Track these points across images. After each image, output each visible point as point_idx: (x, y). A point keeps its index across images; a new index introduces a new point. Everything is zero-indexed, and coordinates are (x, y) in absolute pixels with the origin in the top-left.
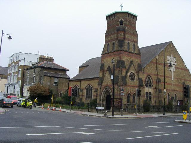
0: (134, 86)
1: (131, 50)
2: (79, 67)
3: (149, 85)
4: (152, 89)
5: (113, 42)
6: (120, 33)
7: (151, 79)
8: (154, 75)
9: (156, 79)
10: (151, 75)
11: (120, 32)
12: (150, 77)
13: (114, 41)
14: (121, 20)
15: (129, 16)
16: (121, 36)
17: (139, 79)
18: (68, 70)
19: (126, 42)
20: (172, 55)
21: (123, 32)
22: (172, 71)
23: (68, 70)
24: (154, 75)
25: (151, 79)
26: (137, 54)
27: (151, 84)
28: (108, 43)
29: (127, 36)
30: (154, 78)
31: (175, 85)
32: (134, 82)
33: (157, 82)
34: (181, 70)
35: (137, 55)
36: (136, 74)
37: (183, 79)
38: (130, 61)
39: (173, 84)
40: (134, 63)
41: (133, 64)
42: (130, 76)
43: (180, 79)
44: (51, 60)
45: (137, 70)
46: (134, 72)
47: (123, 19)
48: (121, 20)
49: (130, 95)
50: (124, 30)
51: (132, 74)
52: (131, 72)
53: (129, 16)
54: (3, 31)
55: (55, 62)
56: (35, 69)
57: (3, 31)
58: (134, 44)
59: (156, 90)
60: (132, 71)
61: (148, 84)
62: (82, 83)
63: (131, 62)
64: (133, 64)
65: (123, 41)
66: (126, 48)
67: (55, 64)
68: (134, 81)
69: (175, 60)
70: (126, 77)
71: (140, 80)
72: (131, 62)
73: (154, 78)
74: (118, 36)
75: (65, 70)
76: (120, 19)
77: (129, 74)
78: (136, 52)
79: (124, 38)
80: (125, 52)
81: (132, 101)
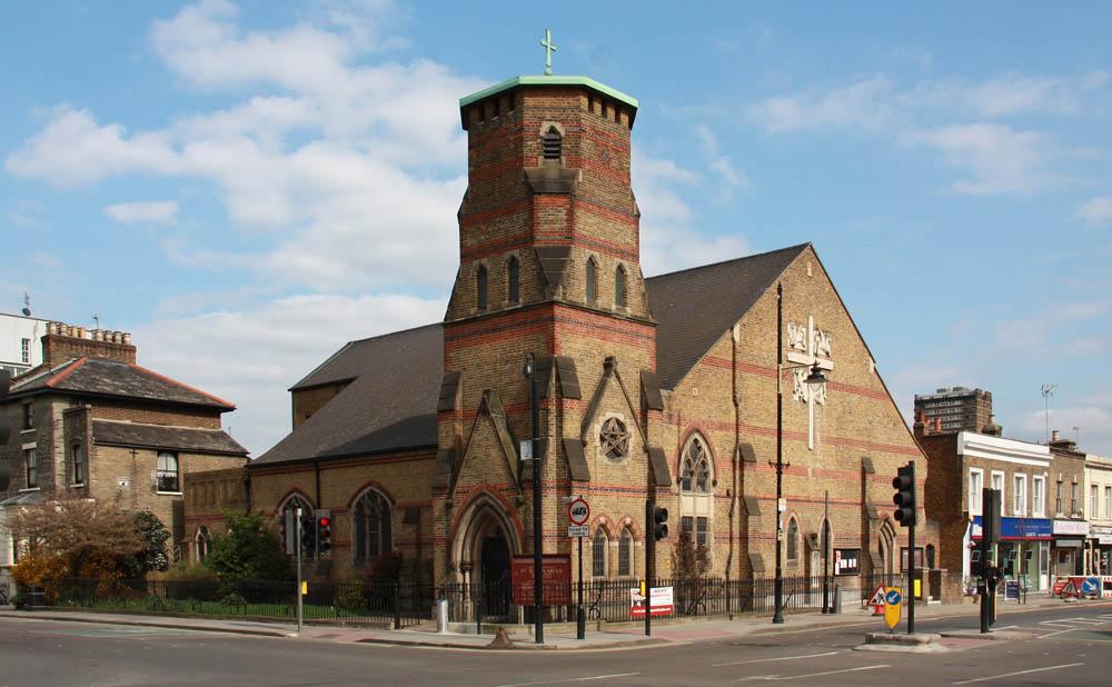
0: (623, 490)
1: (607, 300)
2: (295, 391)
4: (712, 498)
5: (507, 255)
6: (547, 204)
7: (704, 447)
8: (722, 427)
9: (731, 447)
10: (703, 429)
11: (544, 199)
12: (702, 442)
13: (516, 253)
14: (553, 130)
15: (591, 108)
16: (552, 222)
17: (646, 450)
18: (230, 409)
19: (580, 257)
21: (561, 201)
22: (811, 404)
23: (230, 409)
24: (722, 427)
25: (704, 447)
26: (634, 320)
27: (706, 474)
28: (476, 263)
29: (587, 223)
30: (721, 445)
31: (826, 473)
32: (624, 468)
33: (734, 462)
34: (855, 398)
35: (635, 327)
36: (631, 429)
37: (862, 443)
38: (600, 360)
39: (814, 472)
40: (620, 367)
41: (618, 378)
42: (602, 439)
43: (849, 442)
44: (119, 348)
45: (637, 406)
46: (621, 418)
47: (563, 122)
48: (553, 130)
49: (608, 532)
50: (565, 189)
51: (611, 425)
52: (609, 415)
53: (591, 108)
55: (144, 360)
56: (27, 407)
58: (620, 269)
59: (733, 505)
60: (614, 409)
61: (692, 473)
62: (328, 477)
63: (609, 364)
64: (618, 378)
65: (566, 251)
66: (578, 290)
67: (148, 376)
68: (625, 462)
69: (825, 344)
70: (584, 444)
71: (654, 458)
72: (609, 364)
73: (721, 445)
74: (531, 221)
75: (214, 410)
76: (546, 127)
77: (596, 428)
78: (628, 310)
79: (569, 234)
80: (573, 313)
81: (616, 566)
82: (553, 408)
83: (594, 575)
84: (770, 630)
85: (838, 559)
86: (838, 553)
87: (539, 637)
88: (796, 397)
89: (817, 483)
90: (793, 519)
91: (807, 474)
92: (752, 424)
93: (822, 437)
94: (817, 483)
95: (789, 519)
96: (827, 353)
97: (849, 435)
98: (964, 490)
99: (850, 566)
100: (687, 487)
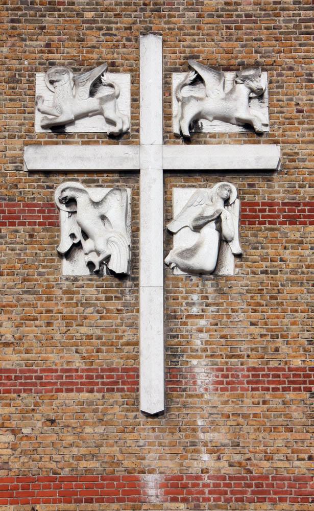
20: (151, 51)
54: (54, 92)
88: (76, 268)
96: (248, 125)
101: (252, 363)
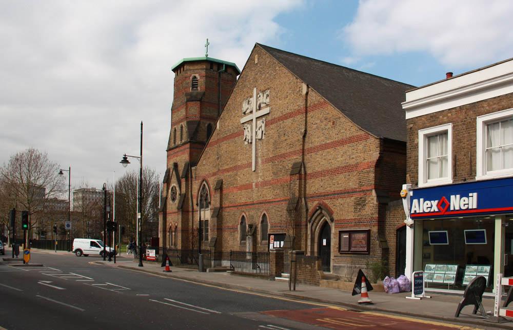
3: (204, 202)
31: (265, 183)
39: (257, 185)
41: (351, 140)
43: (283, 156)
52: (172, 185)
54: (142, 124)
57: (142, 124)
64: (351, 140)
82: (190, 182)
83: (283, 253)
84: (162, 275)
85: (272, 241)
86: (272, 237)
87: (141, 265)
89: (258, 191)
90: (264, 215)
91: (251, 187)
92: (224, 168)
93: (262, 160)
94: (258, 191)
95: (241, 217)
97: (283, 151)
98: (410, 162)
99: (278, 242)
100: (202, 207)
101: (266, 157)
